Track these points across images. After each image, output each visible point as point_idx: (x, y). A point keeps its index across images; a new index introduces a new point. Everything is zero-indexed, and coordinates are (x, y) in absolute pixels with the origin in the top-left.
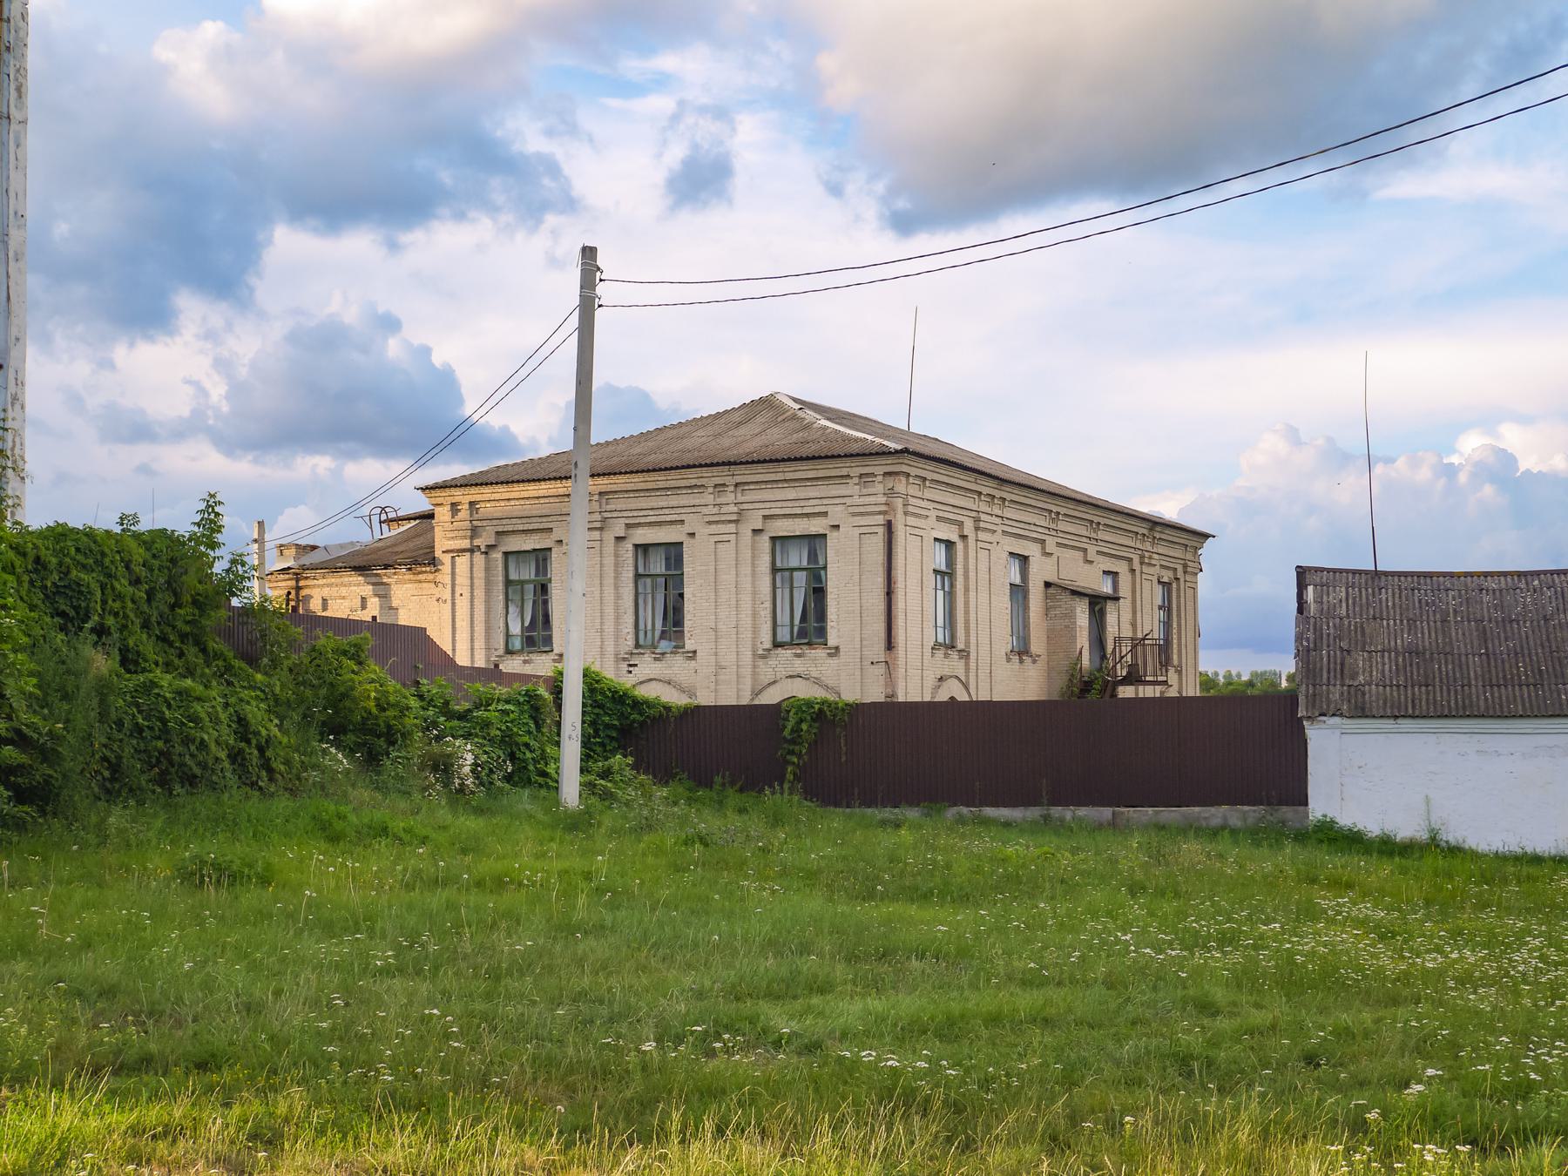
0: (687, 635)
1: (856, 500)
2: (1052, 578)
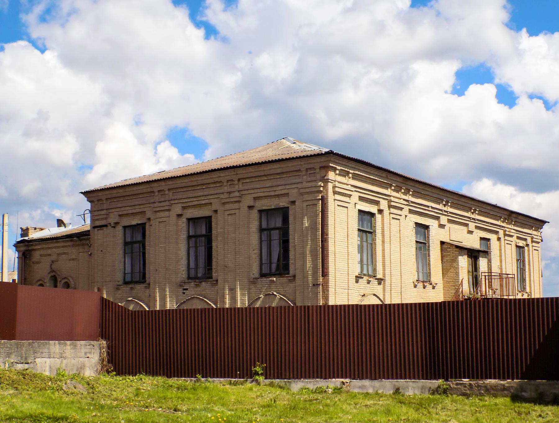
0: (214, 271)
1: (305, 185)
2: (446, 240)
